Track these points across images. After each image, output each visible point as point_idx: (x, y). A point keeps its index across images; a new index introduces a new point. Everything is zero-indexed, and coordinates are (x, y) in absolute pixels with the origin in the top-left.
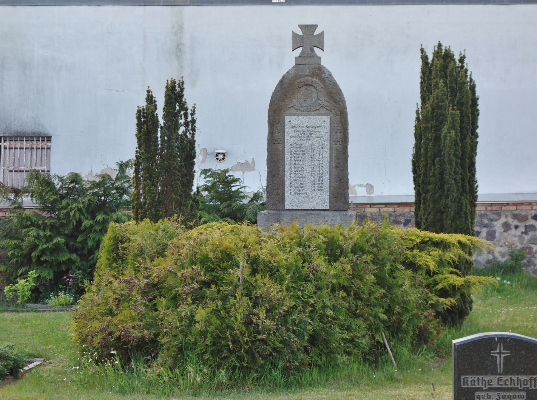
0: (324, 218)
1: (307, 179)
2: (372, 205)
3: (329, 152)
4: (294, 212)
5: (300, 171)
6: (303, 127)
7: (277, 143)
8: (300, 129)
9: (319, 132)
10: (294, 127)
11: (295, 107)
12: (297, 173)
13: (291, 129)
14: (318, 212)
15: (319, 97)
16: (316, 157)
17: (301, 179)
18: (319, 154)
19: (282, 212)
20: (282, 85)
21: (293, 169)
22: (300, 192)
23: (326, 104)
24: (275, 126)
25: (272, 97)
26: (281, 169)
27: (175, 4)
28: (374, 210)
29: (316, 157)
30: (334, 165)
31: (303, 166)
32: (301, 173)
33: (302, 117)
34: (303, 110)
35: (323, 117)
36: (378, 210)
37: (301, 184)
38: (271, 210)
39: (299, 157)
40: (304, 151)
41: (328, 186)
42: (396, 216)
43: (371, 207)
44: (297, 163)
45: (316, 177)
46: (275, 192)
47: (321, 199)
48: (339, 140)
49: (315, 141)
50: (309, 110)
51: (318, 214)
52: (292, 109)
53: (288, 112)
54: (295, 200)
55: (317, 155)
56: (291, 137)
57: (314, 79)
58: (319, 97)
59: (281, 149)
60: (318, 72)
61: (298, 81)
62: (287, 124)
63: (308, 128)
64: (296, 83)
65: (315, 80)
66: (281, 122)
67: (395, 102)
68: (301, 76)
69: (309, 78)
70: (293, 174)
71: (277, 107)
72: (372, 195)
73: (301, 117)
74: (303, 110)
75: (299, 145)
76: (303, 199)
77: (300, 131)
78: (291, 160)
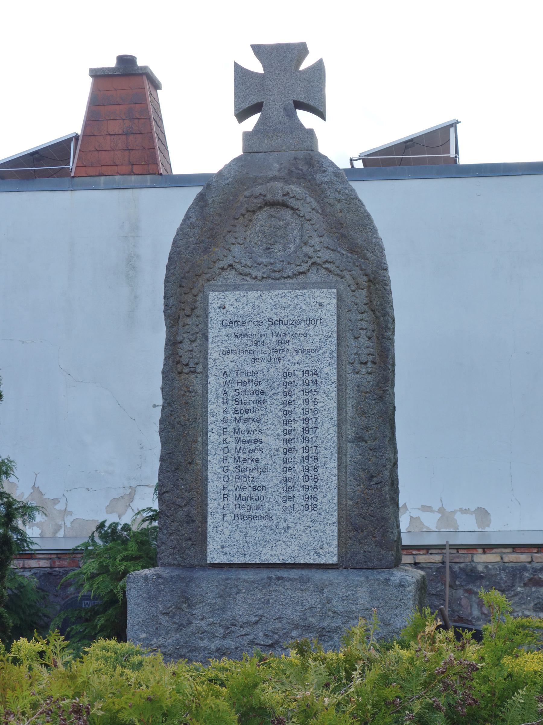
0: (322, 592)
1: (271, 474)
2: (486, 548)
3: (334, 395)
4: (233, 574)
5: (251, 451)
6: (260, 323)
7: (186, 370)
8: (251, 329)
9: (305, 335)
10: (232, 323)
11: (238, 267)
12: (243, 456)
13: (224, 331)
14: (305, 572)
15: (306, 237)
16: (299, 411)
17: (255, 474)
18: (306, 401)
19: (198, 574)
20: (203, 208)
21: (232, 446)
22: (252, 513)
23: (326, 255)
24: (181, 323)
25: (174, 242)
26: (200, 447)
27: (125, 186)
28: (492, 558)
29: (299, 411)
30: (350, 432)
31: (259, 437)
32: (255, 456)
33: (256, 294)
34: (259, 275)
35: (317, 293)
36: (498, 559)
37: (254, 488)
38: (170, 565)
39: (247, 411)
40: (263, 392)
41: (332, 496)
42: (535, 571)
43: (484, 553)
44: (242, 426)
45: (299, 468)
46: (181, 514)
47: (311, 533)
48: (363, 359)
49: (295, 362)
50: (278, 275)
51: (302, 581)
52: (231, 275)
53: (219, 281)
54: (237, 536)
55: (300, 402)
56: (225, 353)
57: (292, 187)
58: (306, 237)
59: (198, 388)
60: (305, 168)
61: (247, 193)
62: (215, 316)
63: (276, 329)
64: (242, 199)
65: (295, 189)
66: (198, 312)
67: (528, 353)
68: (255, 181)
69: (279, 185)
70: (230, 460)
71: (187, 269)
72: (487, 529)
73: (253, 295)
74: (259, 275)
75: (248, 374)
76: (259, 535)
77: (252, 335)
78: (225, 420)
